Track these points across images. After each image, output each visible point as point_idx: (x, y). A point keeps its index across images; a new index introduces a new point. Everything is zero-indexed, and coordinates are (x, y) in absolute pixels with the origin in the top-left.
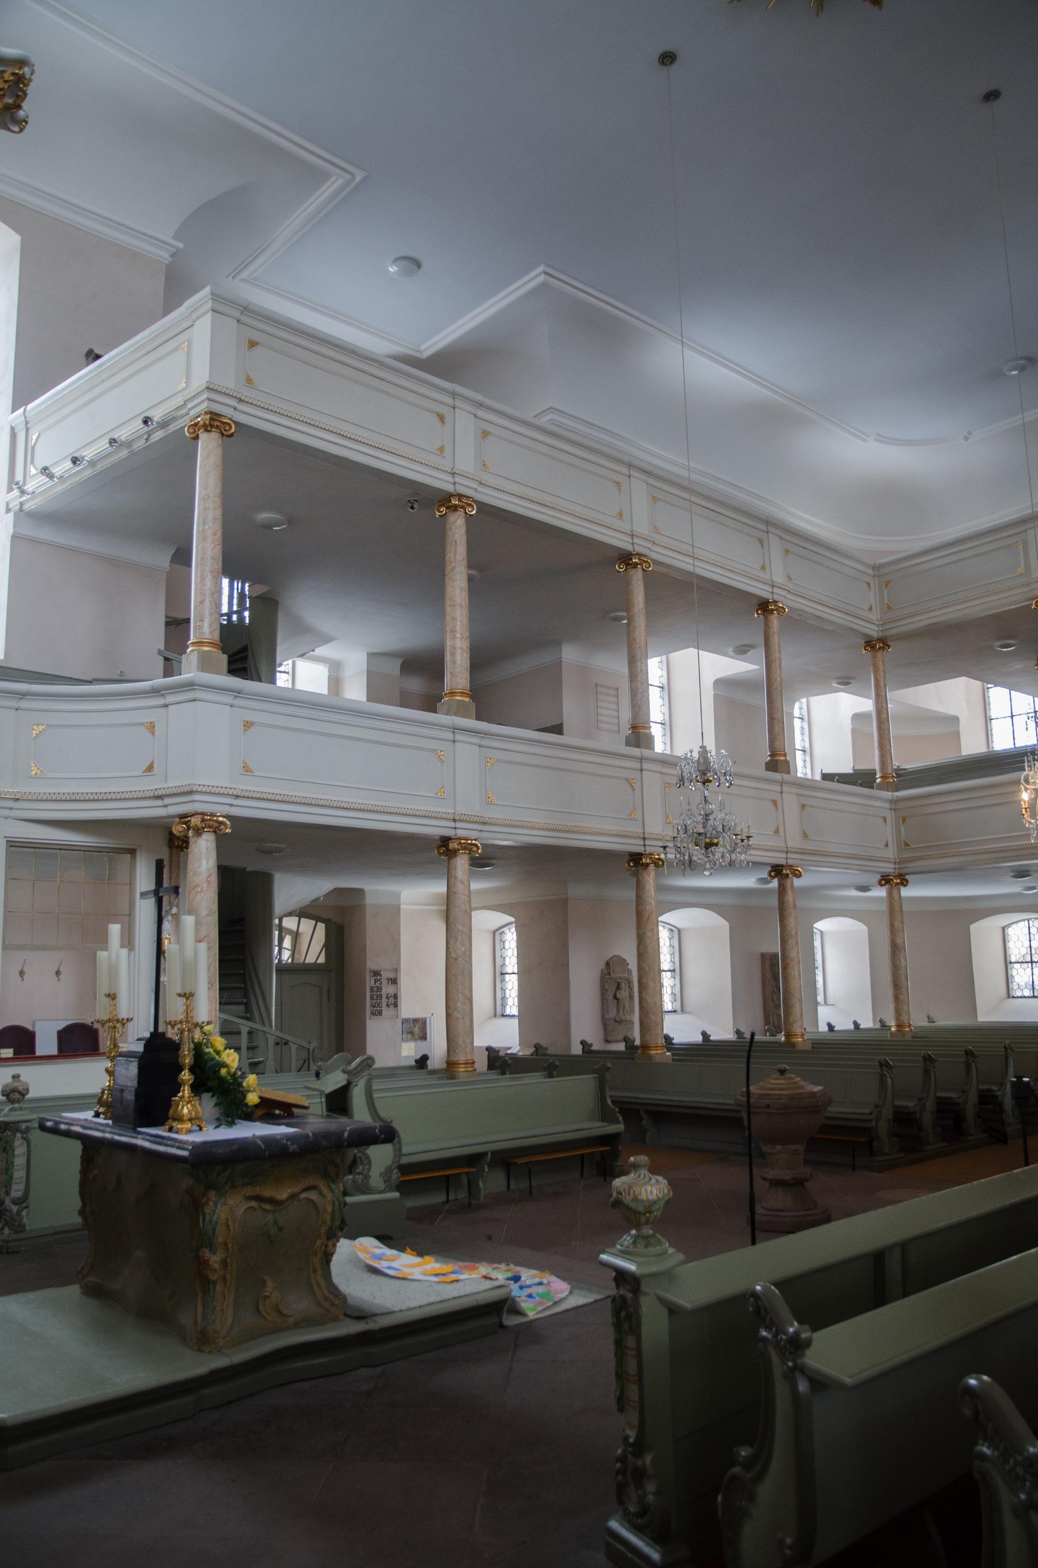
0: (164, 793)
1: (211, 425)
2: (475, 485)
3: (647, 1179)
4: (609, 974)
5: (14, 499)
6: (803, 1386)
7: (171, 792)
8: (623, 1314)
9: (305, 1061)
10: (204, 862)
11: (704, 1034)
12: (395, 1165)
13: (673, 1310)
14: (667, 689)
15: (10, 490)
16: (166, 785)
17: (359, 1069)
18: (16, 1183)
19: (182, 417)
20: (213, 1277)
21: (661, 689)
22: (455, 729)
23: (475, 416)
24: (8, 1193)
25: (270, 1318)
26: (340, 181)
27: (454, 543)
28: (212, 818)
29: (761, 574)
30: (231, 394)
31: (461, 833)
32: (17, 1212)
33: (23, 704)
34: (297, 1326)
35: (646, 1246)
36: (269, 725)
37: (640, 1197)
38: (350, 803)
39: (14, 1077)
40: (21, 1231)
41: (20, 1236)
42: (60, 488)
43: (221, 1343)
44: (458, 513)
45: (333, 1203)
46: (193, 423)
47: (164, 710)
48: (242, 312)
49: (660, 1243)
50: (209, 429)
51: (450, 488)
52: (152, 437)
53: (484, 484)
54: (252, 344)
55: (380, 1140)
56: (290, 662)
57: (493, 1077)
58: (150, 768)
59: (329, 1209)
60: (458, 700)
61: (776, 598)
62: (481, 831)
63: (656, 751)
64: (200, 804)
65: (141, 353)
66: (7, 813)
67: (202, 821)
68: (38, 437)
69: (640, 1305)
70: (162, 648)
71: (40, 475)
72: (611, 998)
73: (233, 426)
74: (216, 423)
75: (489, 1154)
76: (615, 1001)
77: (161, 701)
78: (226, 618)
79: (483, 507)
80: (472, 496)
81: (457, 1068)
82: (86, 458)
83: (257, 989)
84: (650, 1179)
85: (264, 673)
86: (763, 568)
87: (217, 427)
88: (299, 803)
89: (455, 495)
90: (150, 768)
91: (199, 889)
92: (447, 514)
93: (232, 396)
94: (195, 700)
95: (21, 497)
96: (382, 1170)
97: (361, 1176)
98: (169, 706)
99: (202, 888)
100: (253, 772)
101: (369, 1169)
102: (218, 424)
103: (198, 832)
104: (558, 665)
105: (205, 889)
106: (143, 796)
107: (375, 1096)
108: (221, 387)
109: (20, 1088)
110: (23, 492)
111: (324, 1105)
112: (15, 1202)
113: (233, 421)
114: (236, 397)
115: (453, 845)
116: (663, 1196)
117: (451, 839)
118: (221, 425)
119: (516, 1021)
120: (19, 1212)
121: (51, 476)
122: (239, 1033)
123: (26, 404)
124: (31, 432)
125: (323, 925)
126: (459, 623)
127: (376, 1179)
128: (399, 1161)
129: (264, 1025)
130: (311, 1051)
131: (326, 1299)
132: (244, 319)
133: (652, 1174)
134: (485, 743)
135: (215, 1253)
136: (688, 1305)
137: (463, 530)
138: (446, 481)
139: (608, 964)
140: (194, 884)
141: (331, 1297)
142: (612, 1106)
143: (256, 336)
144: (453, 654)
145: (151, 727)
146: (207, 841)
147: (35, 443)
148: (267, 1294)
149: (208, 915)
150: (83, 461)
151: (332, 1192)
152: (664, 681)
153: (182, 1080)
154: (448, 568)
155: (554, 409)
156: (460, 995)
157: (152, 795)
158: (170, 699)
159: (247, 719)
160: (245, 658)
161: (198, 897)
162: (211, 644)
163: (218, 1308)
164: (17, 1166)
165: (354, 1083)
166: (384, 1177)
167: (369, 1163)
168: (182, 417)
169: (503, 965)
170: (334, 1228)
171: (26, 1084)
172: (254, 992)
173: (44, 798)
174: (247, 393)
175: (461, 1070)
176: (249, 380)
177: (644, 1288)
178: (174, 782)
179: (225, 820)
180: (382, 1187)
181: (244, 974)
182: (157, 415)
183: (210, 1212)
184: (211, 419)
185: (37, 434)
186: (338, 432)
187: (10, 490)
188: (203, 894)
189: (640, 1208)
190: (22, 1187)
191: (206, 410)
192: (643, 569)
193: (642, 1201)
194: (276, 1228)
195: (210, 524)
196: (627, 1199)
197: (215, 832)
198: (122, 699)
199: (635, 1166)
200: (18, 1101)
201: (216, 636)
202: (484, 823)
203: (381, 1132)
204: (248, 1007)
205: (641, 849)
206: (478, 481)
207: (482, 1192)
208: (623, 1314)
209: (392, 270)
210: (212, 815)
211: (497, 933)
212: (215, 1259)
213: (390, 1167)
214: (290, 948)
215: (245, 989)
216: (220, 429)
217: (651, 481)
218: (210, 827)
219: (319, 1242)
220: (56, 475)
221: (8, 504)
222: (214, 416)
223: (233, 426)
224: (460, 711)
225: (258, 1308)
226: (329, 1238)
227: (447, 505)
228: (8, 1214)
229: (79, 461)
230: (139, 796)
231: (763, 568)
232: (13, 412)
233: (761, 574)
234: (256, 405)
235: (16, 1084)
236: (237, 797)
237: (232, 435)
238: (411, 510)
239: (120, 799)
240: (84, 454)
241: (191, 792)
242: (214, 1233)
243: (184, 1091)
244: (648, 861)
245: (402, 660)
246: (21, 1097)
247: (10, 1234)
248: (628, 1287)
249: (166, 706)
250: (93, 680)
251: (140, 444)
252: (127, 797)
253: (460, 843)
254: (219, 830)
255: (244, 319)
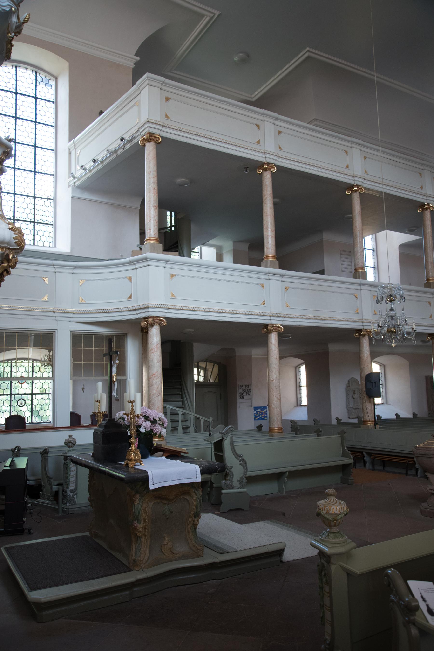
0: (136, 308)
1: (150, 139)
2: (275, 158)
3: (335, 501)
4: (349, 386)
5: (71, 181)
6: (414, 631)
7: (139, 308)
8: (323, 573)
9: (208, 427)
10: (155, 339)
11: (397, 415)
12: (244, 476)
13: (349, 574)
14: (375, 251)
15: (69, 177)
16: (137, 305)
17: (227, 432)
18: (71, 483)
19: (138, 136)
20: (139, 534)
21: (373, 251)
22: (270, 274)
23: (274, 124)
24: (68, 488)
25: (167, 555)
26: (208, 19)
27: (266, 186)
28: (157, 318)
29: (421, 191)
30: (158, 123)
31: (273, 322)
32: (72, 496)
33: (75, 271)
34: (180, 558)
35: (334, 538)
36: (182, 275)
37: (330, 512)
38: (221, 310)
39: (70, 436)
40: (74, 504)
41: (74, 506)
42: (89, 175)
43: (143, 566)
44: (267, 172)
45: (197, 500)
46: (142, 139)
47: (135, 270)
48: (162, 84)
49: (342, 536)
50: (149, 141)
51: (263, 160)
52: (126, 147)
53: (279, 157)
54: (167, 99)
55: (218, 471)
56: (199, 247)
57: (293, 436)
58: (130, 297)
59: (195, 503)
60: (270, 260)
61: (429, 202)
62: (283, 321)
63: (368, 280)
64: (152, 313)
65: (119, 109)
66: (70, 319)
67: (153, 320)
68: (80, 152)
69: (331, 570)
70: (139, 243)
71: (81, 169)
72: (351, 398)
73: (160, 139)
74: (152, 138)
75: (287, 472)
76: (353, 399)
77: (134, 267)
78: (169, 229)
79: (278, 167)
80: (274, 163)
81: (273, 431)
82: (99, 160)
83: (187, 395)
84: (336, 502)
85: (185, 252)
86: (422, 187)
87: (153, 139)
88: (210, 312)
89: (266, 163)
90: (130, 297)
91: (153, 351)
92: (263, 173)
93: (159, 124)
94: (148, 266)
95: (74, 180)
96: (239, 478)
97: (229, 481)
98: (137, 269)
99: (154, 350)
100: (176, 297)
101: (232, 478)
102: (153, 138)
103: (152, 325)
104: (322, 241)
105: (156, 351)
106: (128, 310)
107: (235, 444)
108: (166, 125)
109: (72, 441)
110: (74, 178)
111: (213, 449)
112: (71, 491)
113: (161, 136)
114: (161, 125)
115: (270, 328)
116: (343, 512)
117: (269, 325)
118: (155, 138)
119: (306, 409)
120: (73, 496)
121: (85, 169)
122: (178, 414)
123: (74, 138)
124: (77, 150)
125: (217, 365)
126: (270, 224)
127: (236, 483)
128: (246, 474)
129: (191, 412)
130: (210, 423)
131: (194, 546)
132: (163, 87)
133: (337, 499)
134: (284, 279)
135: (140, 524)
136: (358, 572)
137: (270, 179)
138: (261, 157)
139: (349, 382)
140: (151, 349)
141: (197, 545)
142: (348, 451)
143: (169, 95)
144: (267, 239)
145: (130, 279)
146: (156, 329)
147: (79, 155)
148: (166, 543)
149: (158, 362)
150: (98, 161)
151: (196, 495)
152: (375, 247)
153: (131, 441)
154: (264, 198)
155: (317, 119)
156: (275, 397)
157: (131, 309)
158: (138, 265)
159: (287, 286)
160: (177, 246)
161: (153, 355)
162: (155, 240)
163: (142, 549)
164: (72, 475)
165: (225, 439)
166: (239, 482)
167: (233, 475)
168: (138, 136)
169: (300, 383)
170: (197, 512)
171: (75, 439)
172: (186, 397)
173: (84, 312)
174: (166, 122)
175: (276, 432)
176: (167, 116)
177: (332, 561)
178: (141, 303)
179: (163, 319)
180: (239, 486)
181: (181, 388)
182: (127, 137)
183: (137, 504)
184: (150, 136)
185: (79, 151)
186: (209, 137)
187: (69, 177)
188: (155, 353)
189: (331, 518)
190: (74, 485)
191: (148, 132)
192: (360, 193)
193: (331, 514)
194: (169, 512)
195: (152, 185)
196: (323, 512)
197: (159, 325)
198: (117, 267)
199: (329, 495)
200: (72, 447)
201: (157, 236)
202: (285, 317)
203: (219, 467)
204: (183, 403)
205: (361, 327)
206: (276, 156)
207: (284, 491)
208: (323, 573)
209: (236, 60)
210: (158, 317)
211: (297, 368)
212: (140, 526)
213: (242, 477)
214: (203, 376)
215: (182, 395)
216: (154, 140)
217: (363, 149)
218: (157, 323)
219: (190, 519)
220: (87, 169)
221: (69, 183)
222: (151, 135)
223: (160, 139)
224: (272, 266)
225: (161, 550)
226: (195, 517)
227: (262, 168)
228: (68, 497)
229: (96, 161)
230: (126, 310)
231: (422, 187)
232: (69, 142)
233: (421, 191)
234: (178, 130)
235: (70, 440)
236: (169, 309)
237: (160, 143)
238: (246, 172)
239: (118, 312)
240: (98, 158)
241: (148, 307)
242: (139, 514)
243: (132, 446)
244: (365, 333)
245: (249, 244)
246: (73, 445)
247: (69, 505)
248: (325, 559)
249: (136, 269)
250: (109, 259)
251: (121, 151)
252: (121, 310)
253: (273, 327)
254: (161, 324)
255: (163, 87)
